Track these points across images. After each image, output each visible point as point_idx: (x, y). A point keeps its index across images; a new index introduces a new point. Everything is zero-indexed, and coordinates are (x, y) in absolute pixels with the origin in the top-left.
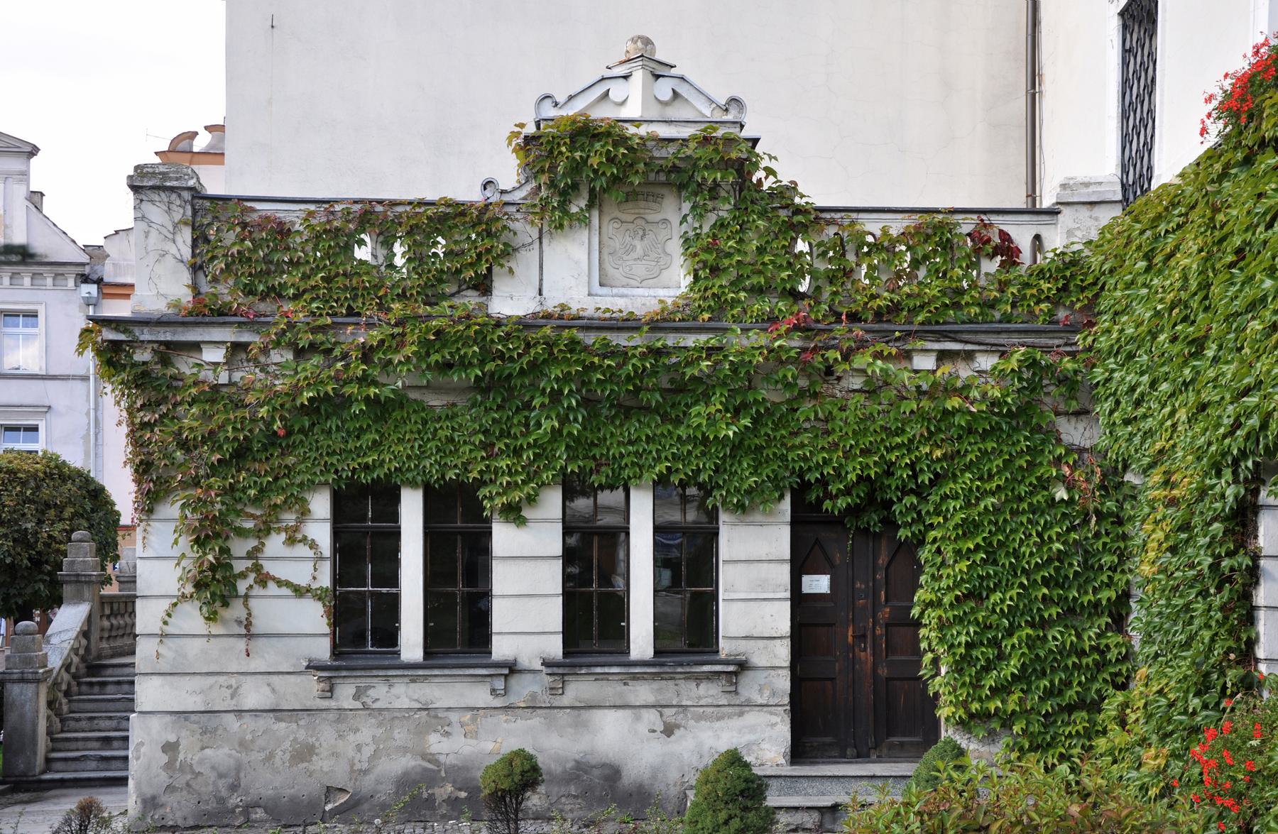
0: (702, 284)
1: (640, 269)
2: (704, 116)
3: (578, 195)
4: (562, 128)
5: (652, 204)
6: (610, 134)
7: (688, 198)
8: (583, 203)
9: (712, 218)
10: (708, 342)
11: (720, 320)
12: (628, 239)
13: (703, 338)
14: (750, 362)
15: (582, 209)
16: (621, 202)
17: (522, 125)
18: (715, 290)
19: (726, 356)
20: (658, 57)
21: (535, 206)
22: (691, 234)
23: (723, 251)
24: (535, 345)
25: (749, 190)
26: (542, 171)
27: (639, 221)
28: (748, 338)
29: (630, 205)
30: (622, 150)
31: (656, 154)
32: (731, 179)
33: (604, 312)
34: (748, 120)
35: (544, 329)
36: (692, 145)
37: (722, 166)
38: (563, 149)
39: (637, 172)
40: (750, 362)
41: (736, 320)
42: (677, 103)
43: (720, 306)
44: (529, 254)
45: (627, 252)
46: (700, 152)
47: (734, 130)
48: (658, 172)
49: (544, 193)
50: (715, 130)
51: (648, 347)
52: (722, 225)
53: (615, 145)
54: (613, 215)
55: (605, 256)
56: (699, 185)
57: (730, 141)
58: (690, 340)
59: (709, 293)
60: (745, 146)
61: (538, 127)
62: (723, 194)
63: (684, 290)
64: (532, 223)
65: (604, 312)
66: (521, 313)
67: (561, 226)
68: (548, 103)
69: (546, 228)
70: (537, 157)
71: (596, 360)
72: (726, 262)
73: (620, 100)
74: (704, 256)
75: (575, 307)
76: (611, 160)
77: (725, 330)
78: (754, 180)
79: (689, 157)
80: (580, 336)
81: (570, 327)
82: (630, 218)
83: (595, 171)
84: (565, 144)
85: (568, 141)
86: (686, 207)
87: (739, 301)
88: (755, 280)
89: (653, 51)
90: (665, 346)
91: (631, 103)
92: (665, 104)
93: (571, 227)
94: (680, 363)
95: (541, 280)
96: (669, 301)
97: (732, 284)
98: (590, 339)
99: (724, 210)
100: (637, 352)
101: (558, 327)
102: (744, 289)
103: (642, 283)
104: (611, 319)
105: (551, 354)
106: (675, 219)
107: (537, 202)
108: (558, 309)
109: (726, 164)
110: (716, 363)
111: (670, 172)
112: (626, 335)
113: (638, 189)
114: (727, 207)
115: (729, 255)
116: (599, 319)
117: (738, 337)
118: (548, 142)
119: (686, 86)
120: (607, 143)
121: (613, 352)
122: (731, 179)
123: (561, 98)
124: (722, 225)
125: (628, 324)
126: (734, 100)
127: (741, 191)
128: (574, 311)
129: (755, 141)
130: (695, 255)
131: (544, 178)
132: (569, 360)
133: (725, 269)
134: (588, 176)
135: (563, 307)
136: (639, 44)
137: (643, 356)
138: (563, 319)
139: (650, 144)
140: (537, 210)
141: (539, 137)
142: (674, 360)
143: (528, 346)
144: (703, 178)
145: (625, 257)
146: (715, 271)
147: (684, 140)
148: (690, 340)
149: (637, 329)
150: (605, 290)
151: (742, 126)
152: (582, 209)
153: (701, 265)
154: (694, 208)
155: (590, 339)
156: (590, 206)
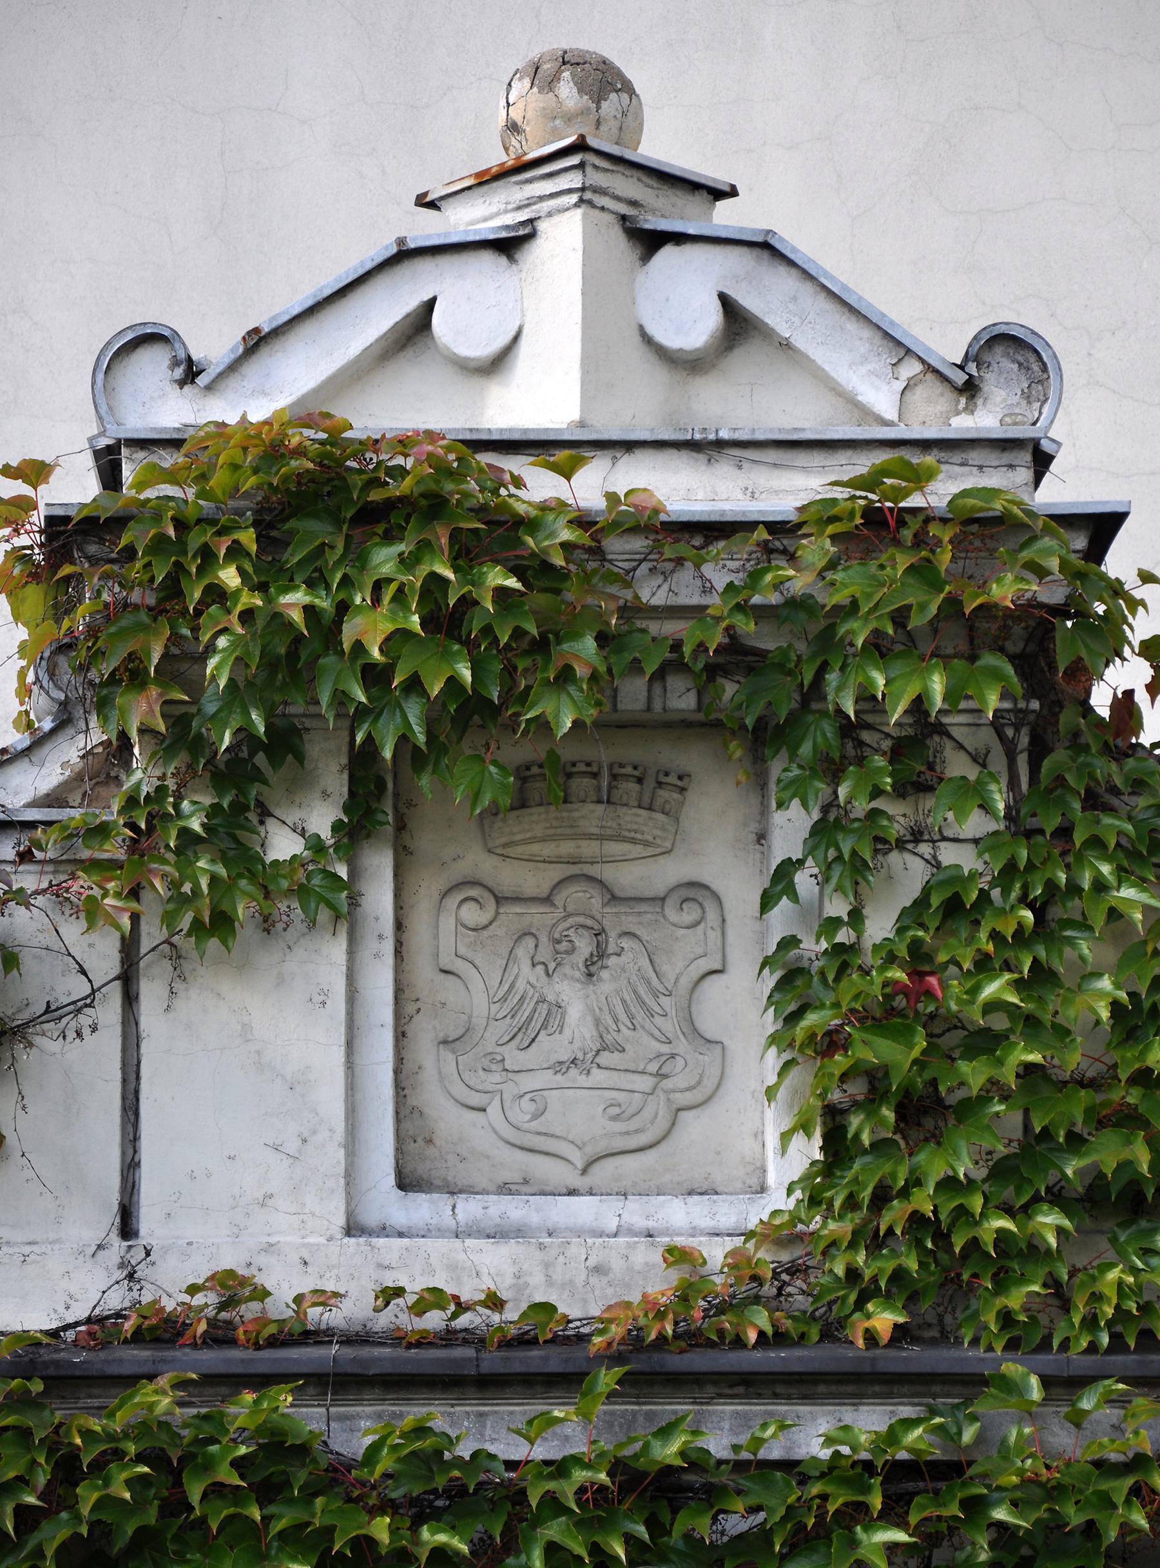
0: (864, 1174)
1: (581, 1112)
2: (866, 414)
3: (301, 783)
4: (219, 480)
5: (633, 818)
6: (448, 502)
7: (796, 790)
8: (322, 819)
9: (909, 875)
10: (892, 1437)
11: (946, 1337)
12: (526, 974)
13: (869, 1421)
14: (1090, 1530)
15: (316, 846)
16: (494, 811)
17: (35, 472)
18: (923, 1202)
19: (975, 1506)
20: (653, 148)
21: (102, 831)
22: (813, 947)
23: (956, 1023)
24: (99, 1465)
25: (1076, 744)
26: (133, 675)
27: (576, 895)
28: (1077, 1420)
29: (536, 821)
30: (498, 578)
31: (653, 593)
32: (993, 701)
33: (420, 1308)
34: (1070, 428)
35: (146, 1394)
36: (816, 549)
37: (953, 639)
38: (229, 577)
39: (566, 675)
40: (1090, 1530)
41: (1018, 1336)
42: (747, 360)
43: (948, 1272)
44: (74, 1050)
45: (525, 1035)
46: (850, 583)
47: (1005, 479)
48: (660, 675)
49: (141, 774)
50: (920, 478)
51: (617, 1467)
52: (950, 905)
53: (466, 554)
54: (462, 869)
55: (424, 1051)
56: (848, 729)
57: (988, 528)
58: (811, 1434)
59: (895, 1215)
60: (1051, 553)
61: (110, 475)
62: (958, 766)
63: (780, 1200)
64: (91, 912)
65: (420, 1308)
66: (37, 1319)
67: (220, 924)
68: (151, 369)
69: (152, 934)
70: (110, 613)
71: (381, 1529)
72: (973, 1074)
73: (481, 348)
74: (873, 1049)
75: (284, 1285)
76: (446, 621)
77: (972, 1383)
78: (1101, 700)
79: (799, 605)
80: (310, 1418)
81: (262, 1381)
82: (534, 880)
83: (375, 676)
84: (236, 552)
85: (248, 538)
86: (791, 826)
87: (1034, 1251)
88: (1109, 1154)
89: (631, 123)
90: (696, 1461)
91: (537, 357)
92: (687, 365)
93: (267, 924)
94: (764, 1535)
95: (130, 1167)
96: (716, 1253)
97: (1001, 1171)
98: (354, 1431)
99: (965, 841)
100: (567, 1490)
101: (210, 1380)
102: (1057, 1197)
103: (590, 1171)
104: (449, 1338)
105: (176, 1504)
106: (740, 888)
107: (112, 814)
108: (207, 1299)
109: (970, 632)
110: (932, 1537)
111: (713, 671)
112: (520, 1411)
113: (568, 754)
114: (976, 824)
115: (985, 1043)
116: (397, 1338)
117: (1029, 1414)
118: (159, 544)
119: (783, 281)
120: (425, 547)
121: (456, 1492)
122: (993, 701)
123: (212, 345)
124: (953, 907)
125: (529, 1358)
126: (1004, 343)
127: (1039, 751)
128: (280, 1306)
129: (1103, 527)
130: (830, 1043)
131: (141, 710)
132: (255, 1532)
133: (969, 1109)
134: (341, 698)
135: (233, 1287)
136: (567, 90)
137: (598, 1506)
138: (233, 1339)
139: (620, 547)
140: (113, 850)
141: (119, 522)
142: (736, 1524)
143: (68, 1470)
144: (866, 698)
145: (514, 1057)
146: (923, 1113)
147: (776, 528)
148: (811, 1434)
149: (567, 1382)
150: (422, 1208)
151: (1042, 461)
152: (316, 846)
153: (858, 1088)
154: (823, 831)
155: (354, 1431)
156: (355, 831)
